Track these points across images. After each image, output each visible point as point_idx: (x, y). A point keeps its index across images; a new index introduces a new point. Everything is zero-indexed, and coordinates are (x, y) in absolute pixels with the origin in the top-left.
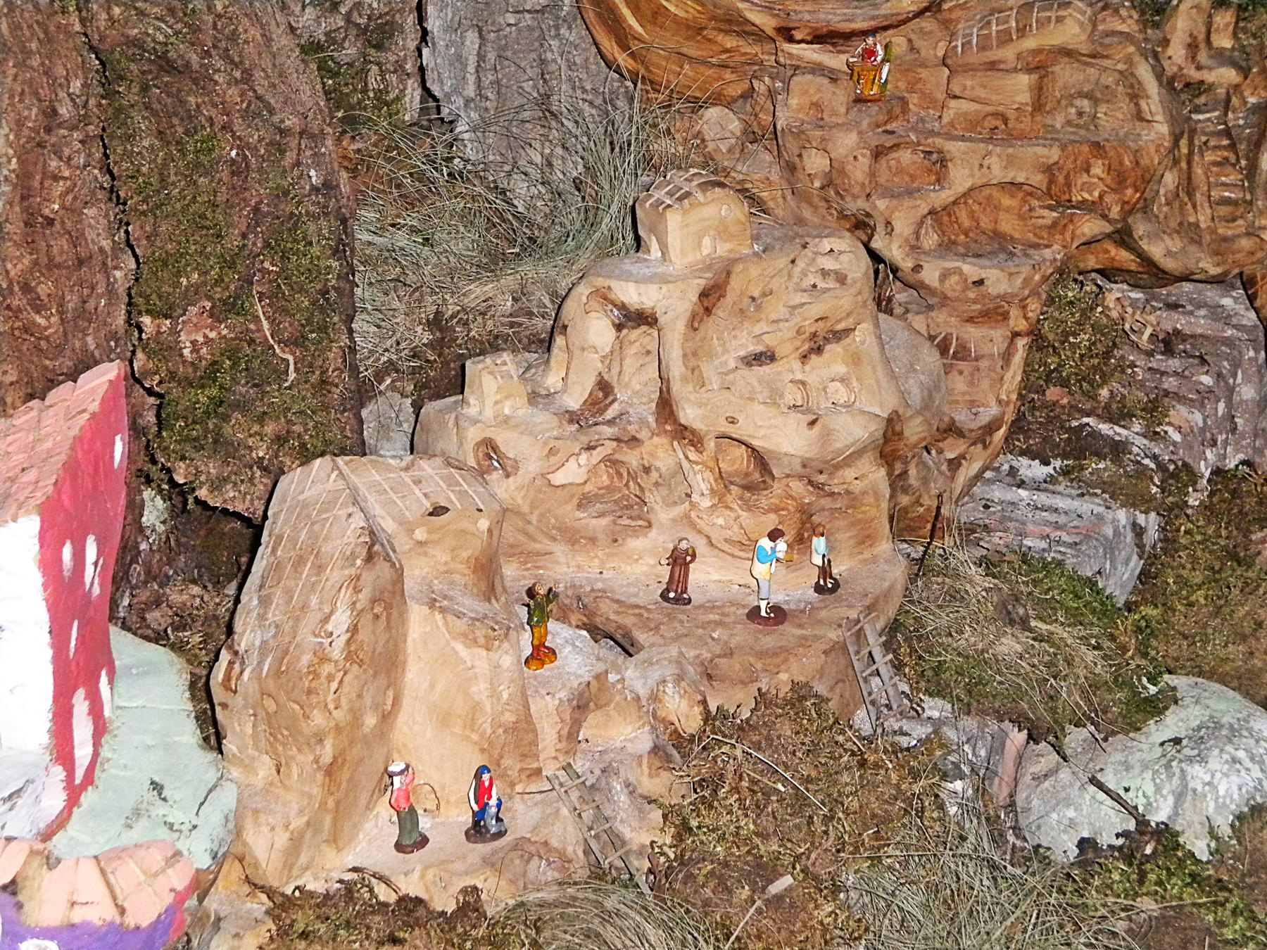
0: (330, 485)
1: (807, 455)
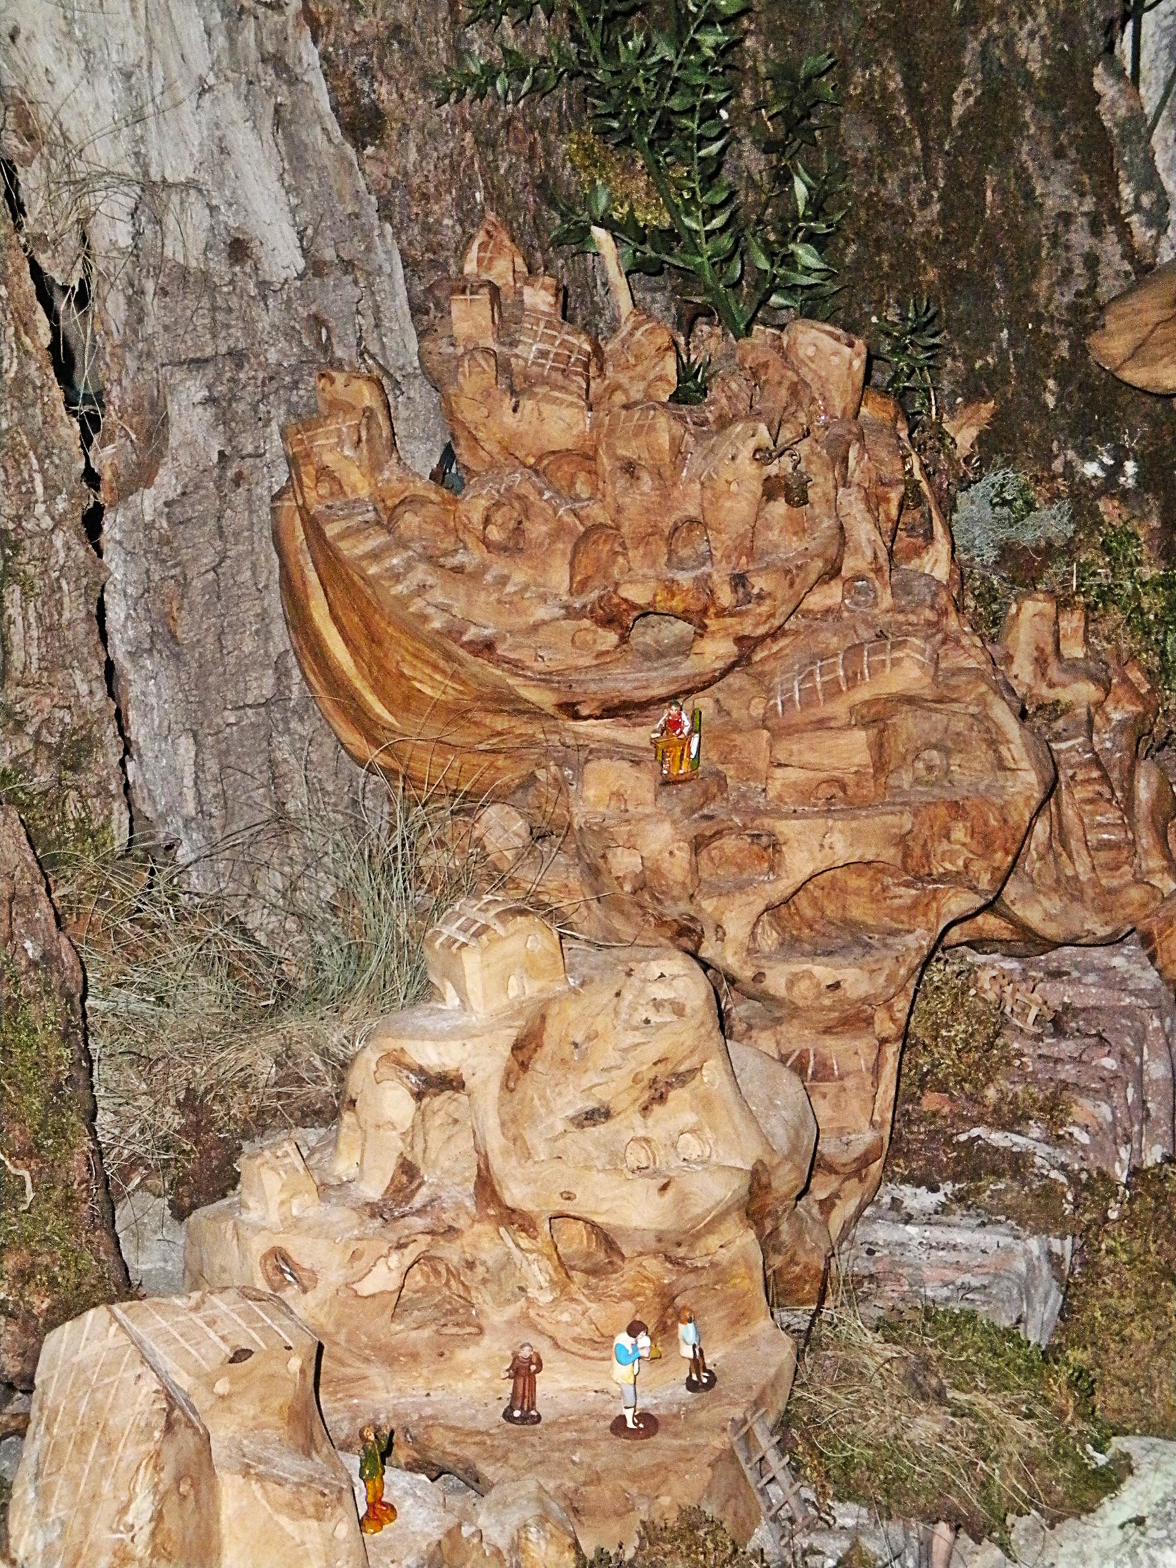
0: (110, 1341)
1: (663, 1227)
